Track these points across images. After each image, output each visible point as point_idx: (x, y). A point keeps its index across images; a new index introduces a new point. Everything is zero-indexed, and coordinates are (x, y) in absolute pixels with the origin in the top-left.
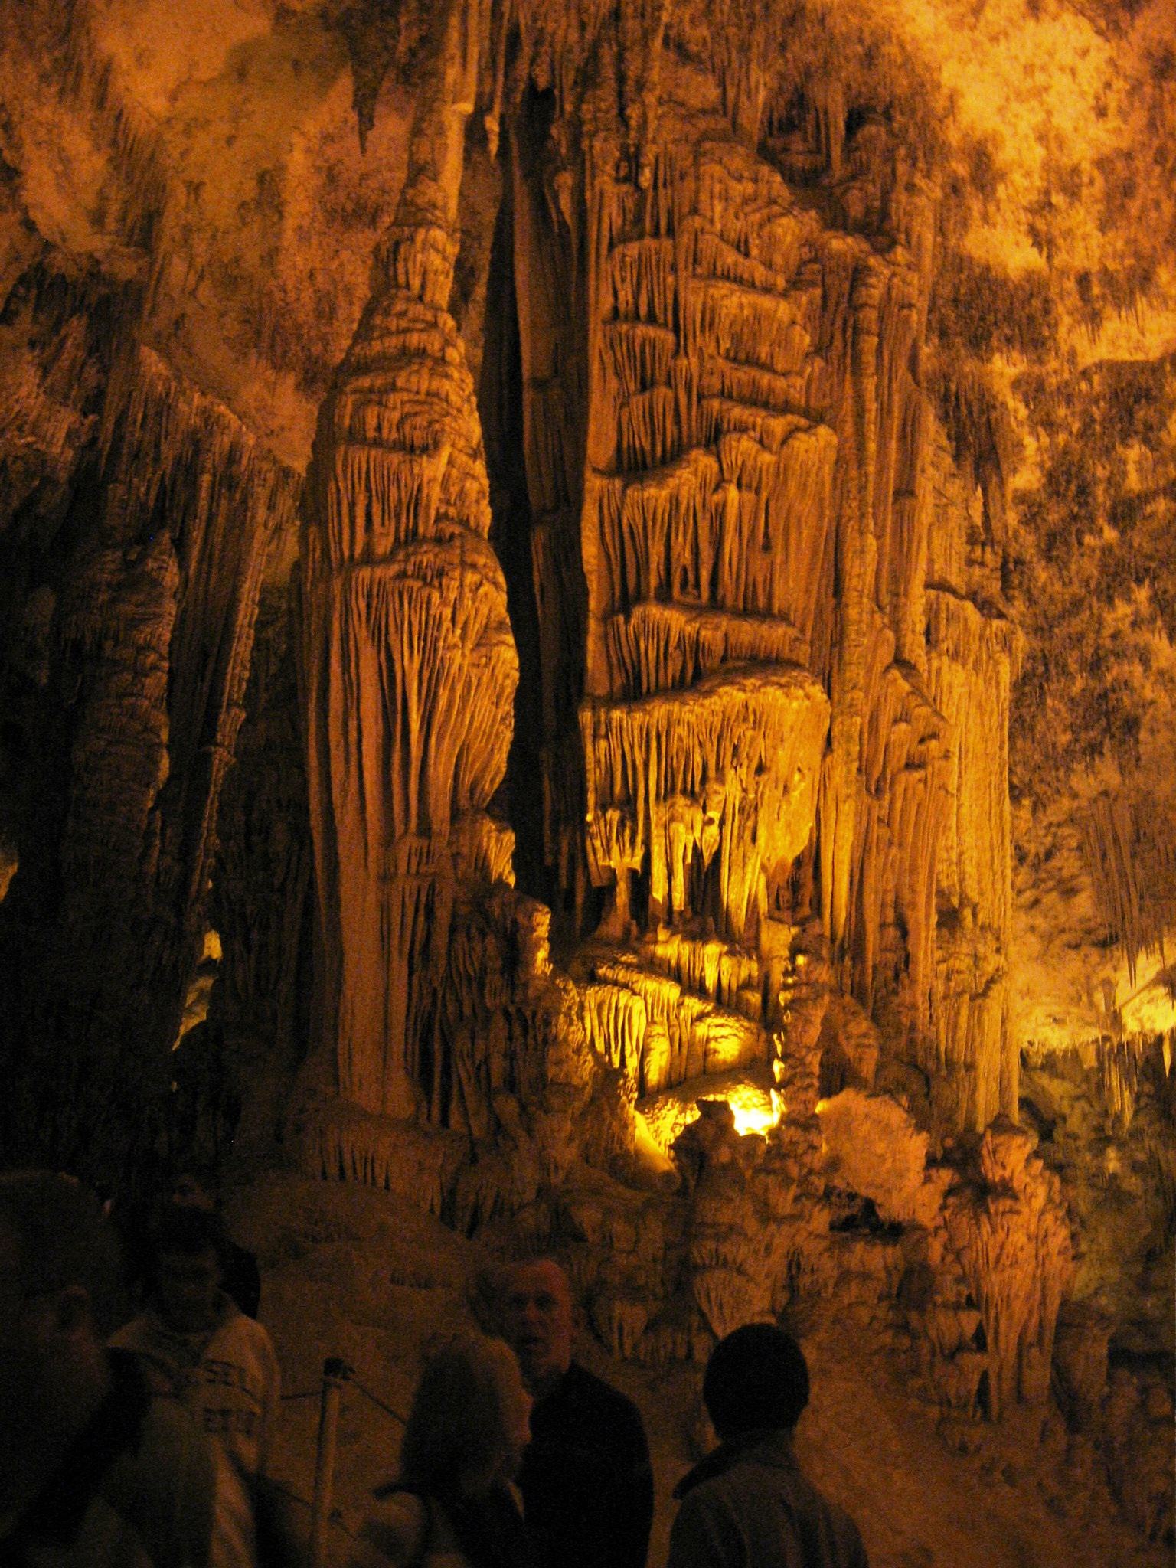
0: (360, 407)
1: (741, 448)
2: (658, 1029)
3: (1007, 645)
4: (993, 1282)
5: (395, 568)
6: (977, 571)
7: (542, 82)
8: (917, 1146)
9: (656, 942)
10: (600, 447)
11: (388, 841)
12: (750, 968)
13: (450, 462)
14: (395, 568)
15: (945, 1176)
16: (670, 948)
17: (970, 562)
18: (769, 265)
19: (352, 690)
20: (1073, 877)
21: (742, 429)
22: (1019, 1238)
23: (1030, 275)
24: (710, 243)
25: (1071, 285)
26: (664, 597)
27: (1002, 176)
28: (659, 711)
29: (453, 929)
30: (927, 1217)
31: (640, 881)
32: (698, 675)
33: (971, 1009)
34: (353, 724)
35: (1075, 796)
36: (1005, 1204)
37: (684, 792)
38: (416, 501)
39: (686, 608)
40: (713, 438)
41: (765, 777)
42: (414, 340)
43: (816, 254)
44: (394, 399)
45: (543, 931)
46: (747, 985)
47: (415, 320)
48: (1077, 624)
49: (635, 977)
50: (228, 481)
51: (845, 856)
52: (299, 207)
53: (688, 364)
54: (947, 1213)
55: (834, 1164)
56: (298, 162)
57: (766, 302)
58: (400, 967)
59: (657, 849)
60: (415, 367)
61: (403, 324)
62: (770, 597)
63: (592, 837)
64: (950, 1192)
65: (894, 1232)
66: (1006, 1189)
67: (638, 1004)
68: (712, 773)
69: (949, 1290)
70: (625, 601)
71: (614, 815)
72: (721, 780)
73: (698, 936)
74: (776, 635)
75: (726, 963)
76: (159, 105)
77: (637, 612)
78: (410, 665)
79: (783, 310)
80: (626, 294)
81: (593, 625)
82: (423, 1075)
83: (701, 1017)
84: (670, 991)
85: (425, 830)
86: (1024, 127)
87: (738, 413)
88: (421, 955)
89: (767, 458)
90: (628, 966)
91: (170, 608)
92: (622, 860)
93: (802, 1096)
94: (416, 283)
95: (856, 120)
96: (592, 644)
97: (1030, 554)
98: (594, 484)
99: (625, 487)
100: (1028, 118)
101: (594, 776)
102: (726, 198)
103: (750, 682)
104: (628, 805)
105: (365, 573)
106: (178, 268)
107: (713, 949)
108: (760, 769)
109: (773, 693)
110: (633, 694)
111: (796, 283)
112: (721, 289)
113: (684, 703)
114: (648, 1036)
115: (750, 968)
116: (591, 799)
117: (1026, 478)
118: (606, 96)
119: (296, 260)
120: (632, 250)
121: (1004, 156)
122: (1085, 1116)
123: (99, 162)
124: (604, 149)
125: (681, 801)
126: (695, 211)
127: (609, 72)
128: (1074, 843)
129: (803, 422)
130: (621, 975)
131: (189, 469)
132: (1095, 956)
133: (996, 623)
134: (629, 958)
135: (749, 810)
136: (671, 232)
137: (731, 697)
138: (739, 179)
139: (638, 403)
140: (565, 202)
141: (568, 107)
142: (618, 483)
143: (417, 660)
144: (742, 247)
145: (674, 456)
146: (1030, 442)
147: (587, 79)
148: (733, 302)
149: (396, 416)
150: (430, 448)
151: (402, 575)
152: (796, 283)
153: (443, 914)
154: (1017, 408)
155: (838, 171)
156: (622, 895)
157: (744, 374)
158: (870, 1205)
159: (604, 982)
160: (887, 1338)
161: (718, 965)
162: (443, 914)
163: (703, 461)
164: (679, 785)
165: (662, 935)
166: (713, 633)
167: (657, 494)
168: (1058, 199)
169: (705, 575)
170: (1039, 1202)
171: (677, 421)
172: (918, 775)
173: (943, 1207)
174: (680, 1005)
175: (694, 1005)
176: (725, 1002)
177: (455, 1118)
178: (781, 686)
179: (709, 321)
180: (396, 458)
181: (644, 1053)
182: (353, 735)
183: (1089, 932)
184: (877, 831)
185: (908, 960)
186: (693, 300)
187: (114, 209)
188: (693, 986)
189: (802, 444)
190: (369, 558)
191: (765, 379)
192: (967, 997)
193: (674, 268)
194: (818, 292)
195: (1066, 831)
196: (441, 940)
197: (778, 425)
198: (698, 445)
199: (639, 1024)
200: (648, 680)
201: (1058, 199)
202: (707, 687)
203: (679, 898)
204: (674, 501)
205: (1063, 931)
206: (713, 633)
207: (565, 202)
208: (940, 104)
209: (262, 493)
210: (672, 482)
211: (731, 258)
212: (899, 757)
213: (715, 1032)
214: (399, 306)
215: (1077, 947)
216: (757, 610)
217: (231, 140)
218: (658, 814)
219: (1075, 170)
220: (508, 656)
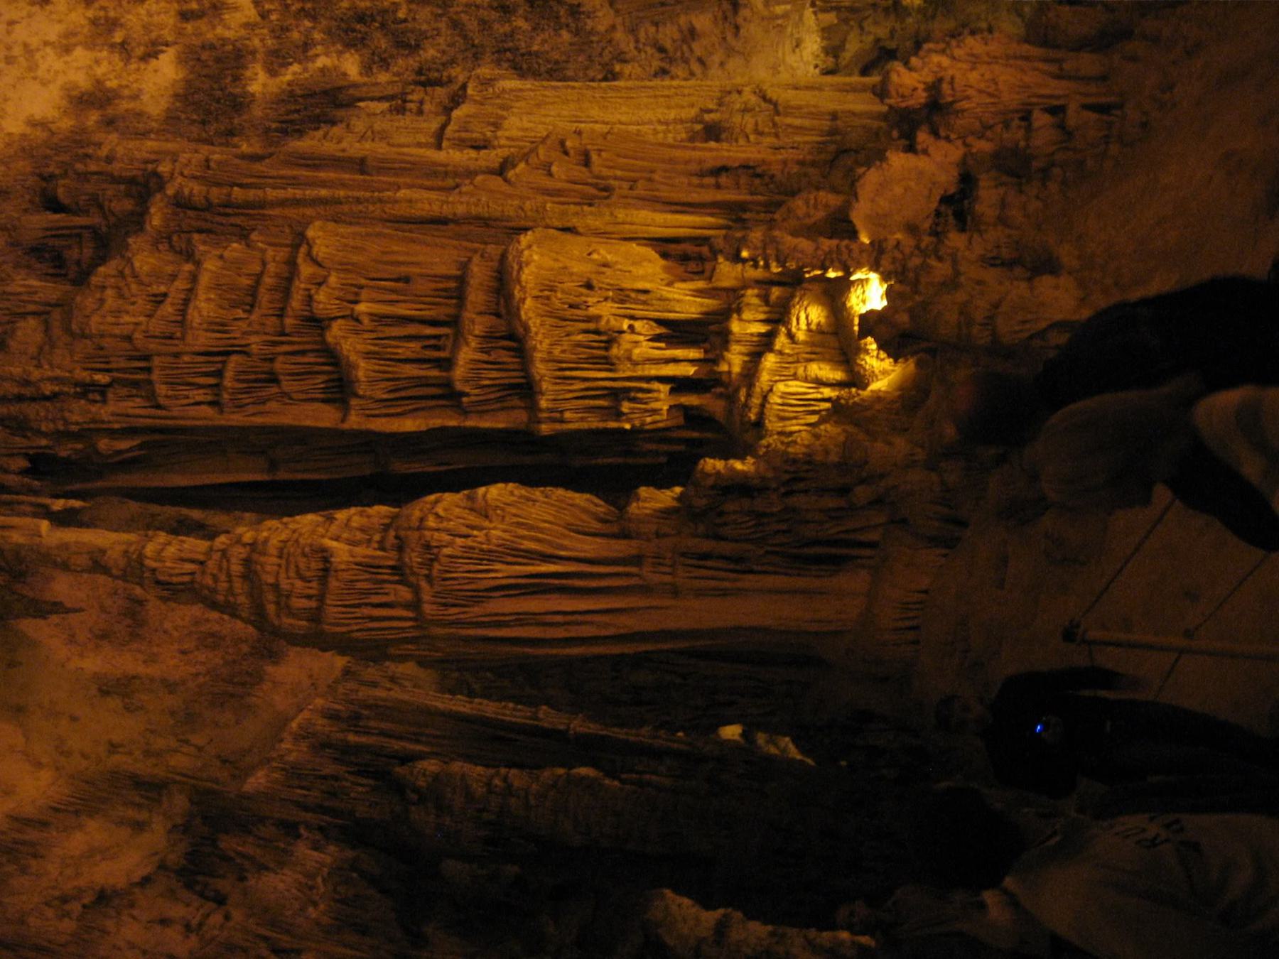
0: (291, 613)
1: (324, 301)
2: (801, 371)
3: (488, 82)
4: (1011, 99)
5: (423, 584)
6: (427, 107)
7: (23, 463)
8: (898, 160)
9: (729, 373)
10: (324, 417)
11: (646, 590)
12: (751, 296)
13: (337, 539)
14: (423, 584)
15: (923, 137)
16: (735, 360)
17: (420, 112)
18: (173, 277)
19: (521, 619)
20: (681, 31)
21: (309, 299)
22: (974, 77)
23: (181, 60)
24: (156, 326)
25: (189, 27)
26: (447, 364)
27: (99, 82)
28: (540, 369)
29: (719, 538)
30: (955, 152)
31: (679, 385)
32: (511, 337)
33: (787, 115)
34: (549, 618)
35: (613, 28)
36: (945, 87)
37: (607, 349)
38: (369, 567)
39: (456, 347)
40: (317, 323)
41: (595, 283)
42: (236, 568)
43: (164, 238)
44: (285, 584)
45: (719, 465)
46: (765, 299)
47: (220, 569)
48: (472, 25)
49: (758, 390)
50: (355, 721)
51: (660, 218)
52: (127, 662)
53: (255, 343)
54: (953, 136)
55: (912, 229)
56: (92, 664)
57: (204, 279)
58: (749, 581)
59: (653, 371)
60: (259, 567)
61: (223, 577)
62: (447, 278)
63: (643, 424)
64: (935, 133)
65: (967, 180)
66: (934, 88)
67: (781, 387)
68: (592, 326)
69: (1015, 135)
70: (450, 396)
71: (626, 407)
72: (597, 318)
73: (725, 338)
74: (479, 273)
75: (747, 315)
76: (46, 776)
77: (459, 386)
78: (502, 572)
79: (211, 265)
80: (199, 395)
81: (470, 423)
82: (836, 563)
83: (791, 336)
84: (770, 361)
85: (637, 560)
86: (58, 65)
87: (296, 303)
88: (740, 564)
89: (333, 280)
90: (749, 395)
91: (457, 766)
92: (662, 399)
93: (855, 254)
94: (189, 567)
95: (53, 205)
96: (486, 423)
97: (413, 62)
98: (355, 421)
99: (357, 396)
100: (50, 61)
101: (594, 423)
102: (118, 312)
103: (517, 294)
104: (617, 395)
105: (428, 609)
106: (181, 761)
107: (735, 327)
108: (589, 286)
109: (527, 275)
110: (526, 390)
111: (189, 255)
112: (194, 317)
113: (535, 349)
114: (806, 380)
115: (751, 296)
116: (613, 425)
117: (351, 66)
118: (31, 410)
119: (171, 664)
120: (162, 390)
121: (82, 81)
122: (876, 23)
123: (92, 825)
124: (78, 413)
125: (614, 351)
126: (129, 338)
127: (14, 409)
128: (653, 29)
129: (303, 250)
130: (756, 401)
131: (344, 752)
132: (744, 12)
133: (470, 91)
134: (742, 394)
135: (622, 296)
136: (147, 358)
137: (529, 310)
138: (102, 301)
139: (287, 385)
140: (124, 445)
141: (44, 442)
142: (354, 402)
143: (498, 566)
144: (159, 299)
145: (332, 356)
146: (322, 62)
147: (20, 426)
148: (204, 307)
149: (299, 584)
150: (324, 555)
151: (428, 578)
152: (189, 255)
153: (707, 546)
154: (293, 72)
155: (95, 219)
156: (691, 400)
157: (264, 297)
158: (946, 200)
159: (761, 415)
160: (1053, 187)
161: (749, 321)
162: (707, 546)
163: (336, 332)
164: (602, 353)
165: (724, 367)
166: (476, 324)
167: (363, 370)
168: (118, 37)
169: (429, 331)
170: (945, 61)
171: (303, 353)
172: (594, 157)
173: (948, 139)
174: (781, 353)
175: (781, 341)
176: (779, 317)
177: (873, 536)
178: (521, 268)
179: (219, 326)
180: (333, 583)
181: (820, 383)
182: (559, 618)
183: (725, 18)
184: (640, 190)
185: (745, 167)
186: (202, 339)
187: (131, 813)
188: (765, 343)
189: (321, 250)
190: (415, 605)
191: (268, 280)
192: (777, 118)
193: (177, 355)
194: (196, 236)
195: (642, 35)
196: (726, 548)
197: (306, 270)
198: (322, 335)
199: (795, 386)
200: (515, 377)
201: (118, 37)
202: (521, 330)
203: (694, 354)
204: (368, 355)
205: (724, 39)
206: (476, 324)
207: (124, 445)
208: (40, 134)
209: (364, 693)
210: (353, 358)
211: (168, 309)
212: (580, 172)
213: (803, 326)
214: (209, 581)
215: (737, 28)
216: (457, 290)
217: (74, 719)
218: (626, 371)
219: (94, 22)
220: (494, 492)
